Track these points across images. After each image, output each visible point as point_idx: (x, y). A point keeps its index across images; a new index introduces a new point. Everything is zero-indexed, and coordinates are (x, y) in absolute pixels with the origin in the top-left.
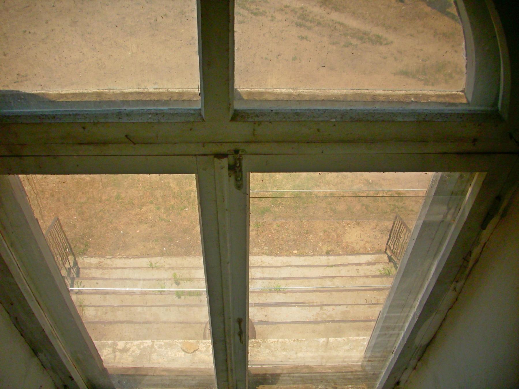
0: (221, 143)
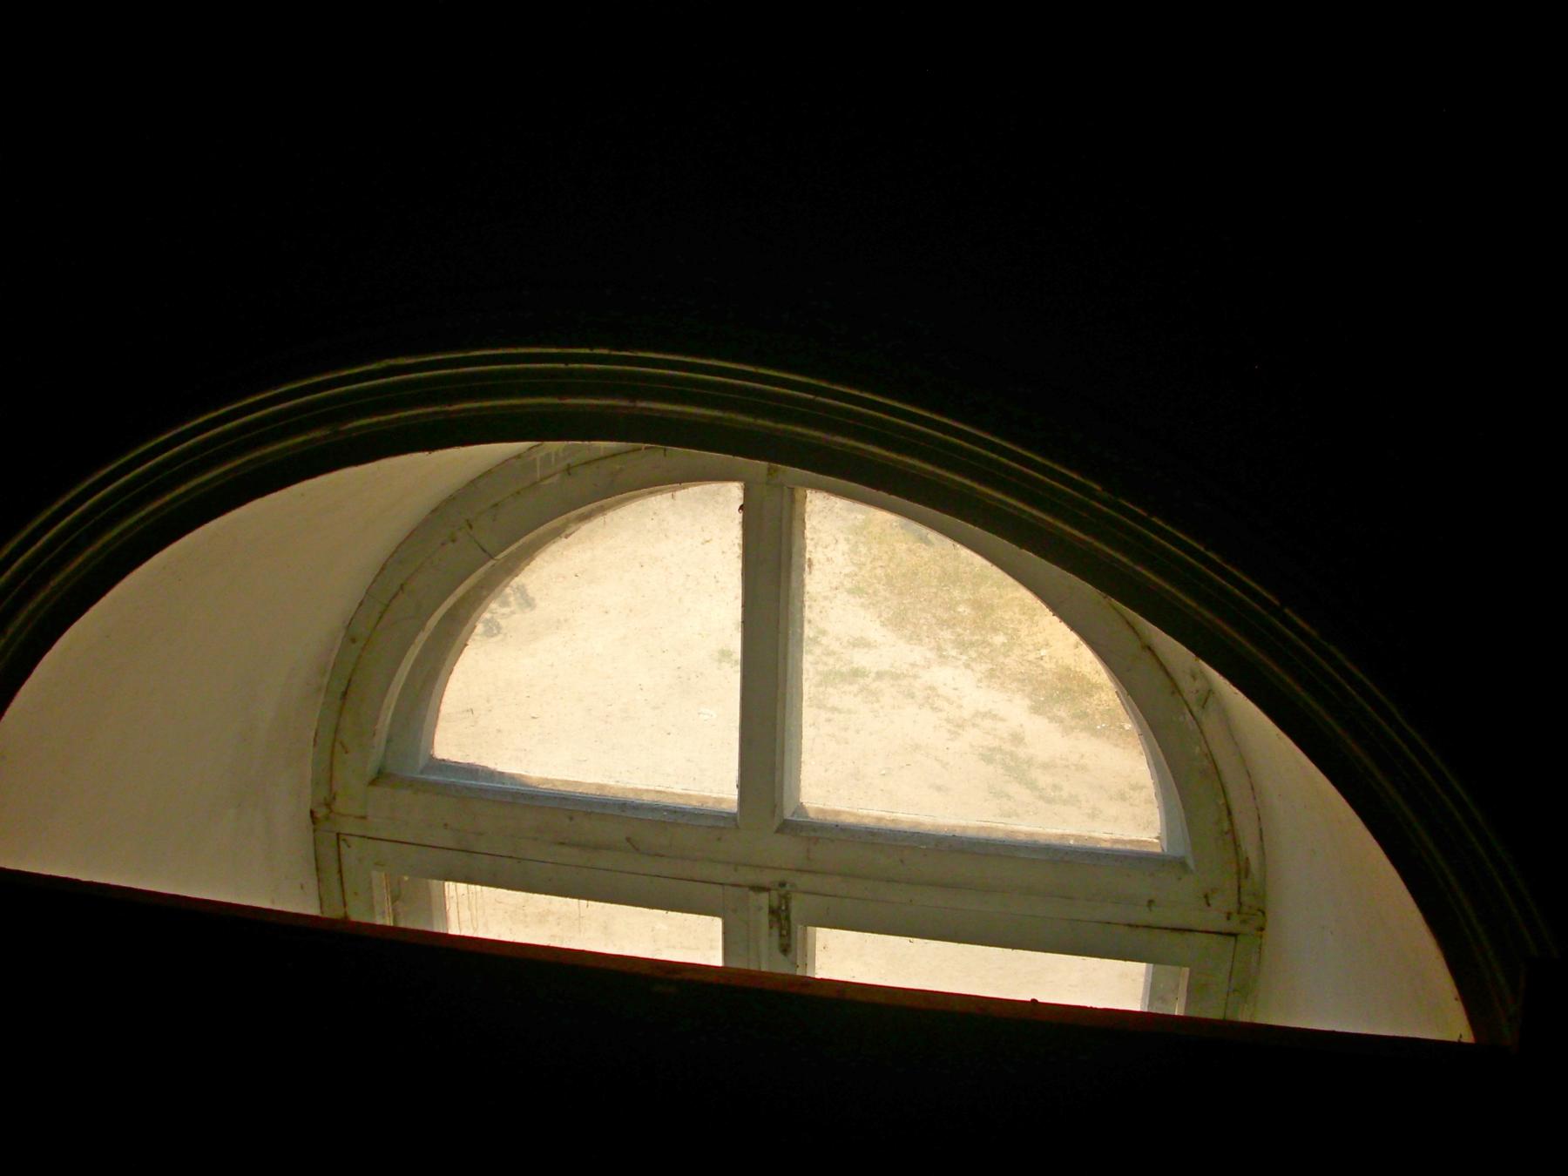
0: (762, 867)
